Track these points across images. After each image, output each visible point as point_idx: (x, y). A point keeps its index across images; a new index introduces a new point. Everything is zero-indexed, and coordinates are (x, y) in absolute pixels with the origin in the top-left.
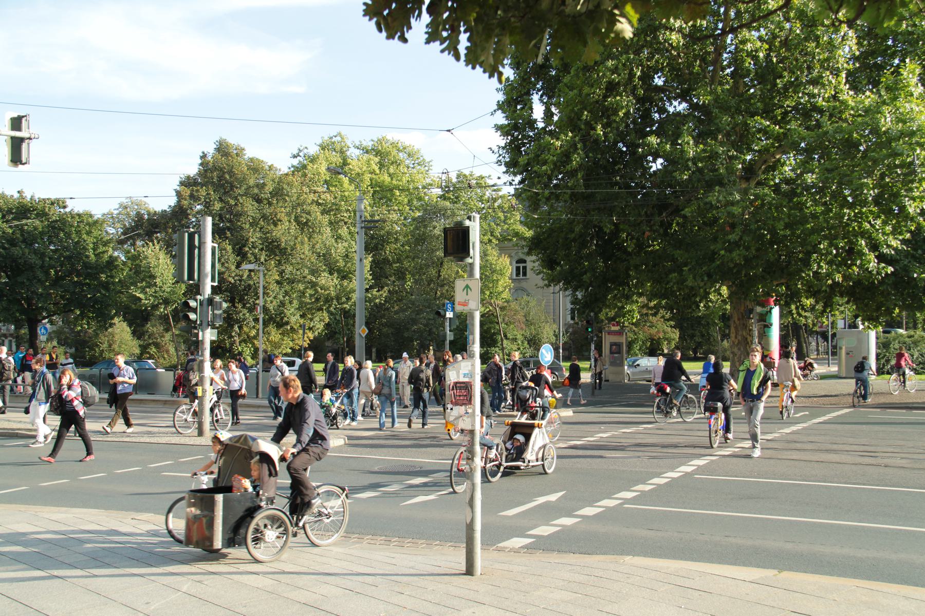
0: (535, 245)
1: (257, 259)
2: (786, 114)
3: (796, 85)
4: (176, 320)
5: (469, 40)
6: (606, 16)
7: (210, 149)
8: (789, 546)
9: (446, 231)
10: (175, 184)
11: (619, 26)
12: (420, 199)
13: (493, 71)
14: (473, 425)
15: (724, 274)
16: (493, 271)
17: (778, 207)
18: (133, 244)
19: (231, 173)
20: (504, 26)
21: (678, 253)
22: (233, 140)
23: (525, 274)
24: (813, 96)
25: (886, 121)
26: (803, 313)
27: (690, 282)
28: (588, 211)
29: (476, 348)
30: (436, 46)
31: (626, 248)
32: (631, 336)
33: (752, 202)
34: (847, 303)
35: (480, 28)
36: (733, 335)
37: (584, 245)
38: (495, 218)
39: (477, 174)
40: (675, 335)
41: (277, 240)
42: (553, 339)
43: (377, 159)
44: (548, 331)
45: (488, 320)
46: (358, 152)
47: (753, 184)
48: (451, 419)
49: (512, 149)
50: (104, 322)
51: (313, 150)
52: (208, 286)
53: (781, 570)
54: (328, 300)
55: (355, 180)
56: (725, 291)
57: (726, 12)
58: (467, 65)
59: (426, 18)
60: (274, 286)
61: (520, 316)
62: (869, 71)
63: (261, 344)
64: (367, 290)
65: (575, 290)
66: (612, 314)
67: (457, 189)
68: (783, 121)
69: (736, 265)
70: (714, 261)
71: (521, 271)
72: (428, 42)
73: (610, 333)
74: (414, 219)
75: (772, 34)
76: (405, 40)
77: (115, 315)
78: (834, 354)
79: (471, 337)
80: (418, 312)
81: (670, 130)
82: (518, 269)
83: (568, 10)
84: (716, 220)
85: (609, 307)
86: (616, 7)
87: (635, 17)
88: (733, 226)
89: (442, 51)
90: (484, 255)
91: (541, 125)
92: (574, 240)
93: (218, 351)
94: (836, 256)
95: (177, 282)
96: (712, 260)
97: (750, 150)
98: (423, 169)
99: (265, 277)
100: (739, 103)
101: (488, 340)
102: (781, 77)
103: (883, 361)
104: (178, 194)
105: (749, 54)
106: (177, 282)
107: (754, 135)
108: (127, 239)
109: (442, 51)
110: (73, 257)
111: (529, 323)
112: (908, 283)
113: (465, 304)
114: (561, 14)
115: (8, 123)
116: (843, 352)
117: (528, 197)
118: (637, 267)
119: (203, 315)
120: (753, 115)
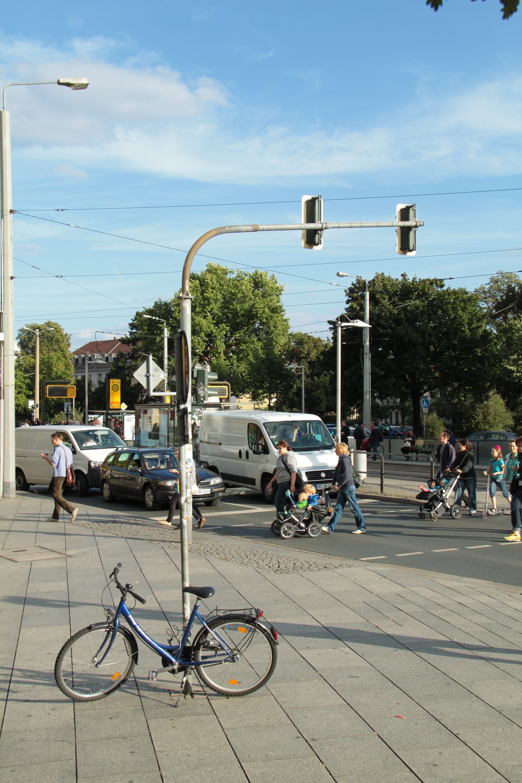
50: (481, 396)
110: (450, 331)
115: (397, 214)
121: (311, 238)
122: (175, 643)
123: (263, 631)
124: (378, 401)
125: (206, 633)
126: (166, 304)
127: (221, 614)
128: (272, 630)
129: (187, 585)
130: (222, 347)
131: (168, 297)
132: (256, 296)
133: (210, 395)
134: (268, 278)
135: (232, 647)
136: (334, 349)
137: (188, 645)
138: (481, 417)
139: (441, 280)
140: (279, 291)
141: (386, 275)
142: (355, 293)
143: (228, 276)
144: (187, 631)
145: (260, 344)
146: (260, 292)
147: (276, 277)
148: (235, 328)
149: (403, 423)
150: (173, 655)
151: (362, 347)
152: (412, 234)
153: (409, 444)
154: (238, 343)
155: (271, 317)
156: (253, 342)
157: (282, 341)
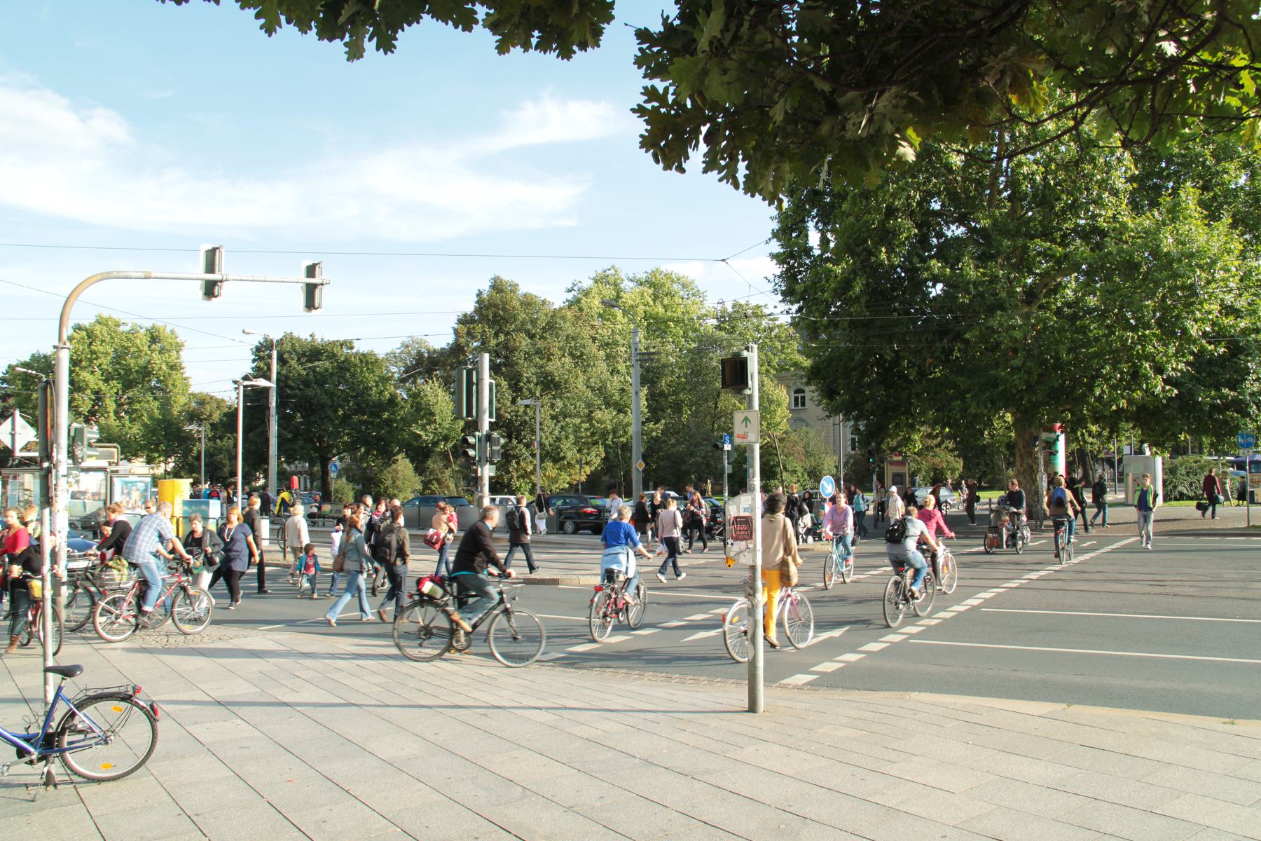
0: (814, 374)
1: (532, 394)
2: (1064, 236)
3: (1074, 208)
4: (456, 457)
5: (747, 168)
6: (887, 140)
7: (485, 287)
8: (1078, 679)
9: (723, 362)
10: (453, 322)
11: (901, 150)
12: (695, 330)
13: (772, 198)
14: (754, 561)
15: (1008, 401)
16: (771, 402)
17: (1061, 330)
18: (414, 382)
19: (504, 309)
20: (783, 153)
21: (960, 380)
22: (506, 277)
23: (803, 404)
24: (1094, 217)
25: (1168, 243)
26: (1090, 440)
27: (973, 410)
28: (867, 339)
29: (757, 481)
30: (714, 175)
31: (907, 376)
32: (914, 466)
33: (1033, 326)
34: (1133, 428)
35: (759, 155)
36: (1018, 464)
37: (865, 373)
38: (772, 348)
39: (753, 303)
40: (959, 465)
41: (551, 374)
42: (834, 471)
43: (651, 291)
44: (829, 462)
45: (767, 451)
46: (631, 284)
47: (1034, 308)
48: (732, 554)
49: (788, 278)
50: (387, 458)
51: (587, 283)
52: (486, 422)
53: (1070, 704)
54: (604, 435)
55: (629, 311)
56: (1009, 417)
57: (1001, 137)
58: (746, 193)
59: (703, 148)
60: (548, 422)
61: (799, 448)
62: (1146, 192)
63: (538, 479)
64: (643, 423)
65: (857, 419)
66: (894, 443)
67: (733, 319)
68: (1063, 244)
69: (1018, 391)
70: (997, 387)
71: (799, 401)
72: (705, 171)
73: (892, 463)
74: (689, 351)
75: (1048, 157)
76: (682, 171)
77: (398, 453)
78: (1121, 481)
79: (751, 471)
80: (697, 444)
81: (953, 253)
82: (796, 399)
83: (848, 135)
84: (998, 344)
85: (890, 436)
86: (898, 131)
87: (917, 140)
88: (1015, 351)
89: (720, 180)
90: (762, 385)
91: (817, 252)
92: (855, 369)
93: (497, 486)
94: (1121, 380)
95: (456, 418)
96: (995, 386)
97: (1031, 272)
98: (697, 300)
99: (541, 412)
100: (1017, 228)
101: (768, 473)
102: (1059, 199)
103: (1170, 487)
104: (456, 332)
105: (1025, 177)
106: (456, 418)
107: (1034, 259)
108: (409, 377)
109: (720, 180)
110: (360, 397)
111: (808, 454)
112: (1193, 407)
113: (744, 436)
114: (841, 139)
115: (303, 271)
116: (1130, 478)
117: (807, 327)
118: (918, 395)
119: (482, 451)
120: (1032, 238)
121: (210, 290)
122: (32, 731)
123: (142, 708)
124: (285, 466)
125: (73, 715)
126: (45, 357)
127: (91, 693)
128: (152, 706)
129: (50, 663)
130: (111, 405)
131: (48, 350)
132: (152, 351)
133: (89, 456)
134: (168, 330)
135: (106, 727)
136: (237, 409)
137: (51, 731)
138: (389, 482)
139: (351, 342)
140: (179, 347)
141: (295, 334)
142: (262, 351)
143: (121, 329)
144: (49, 716)
145: (157, 403)
146: (157, 347)
147: (176, 329)
148: (128, 385)
149: (311, 489)
150: (32, 744)
151: (269, 408)
152: (317, 291)
153: (315, 510)
154: (131, 401)
155: (170, 375)
156: (148, 402)
157: (182, 400)
